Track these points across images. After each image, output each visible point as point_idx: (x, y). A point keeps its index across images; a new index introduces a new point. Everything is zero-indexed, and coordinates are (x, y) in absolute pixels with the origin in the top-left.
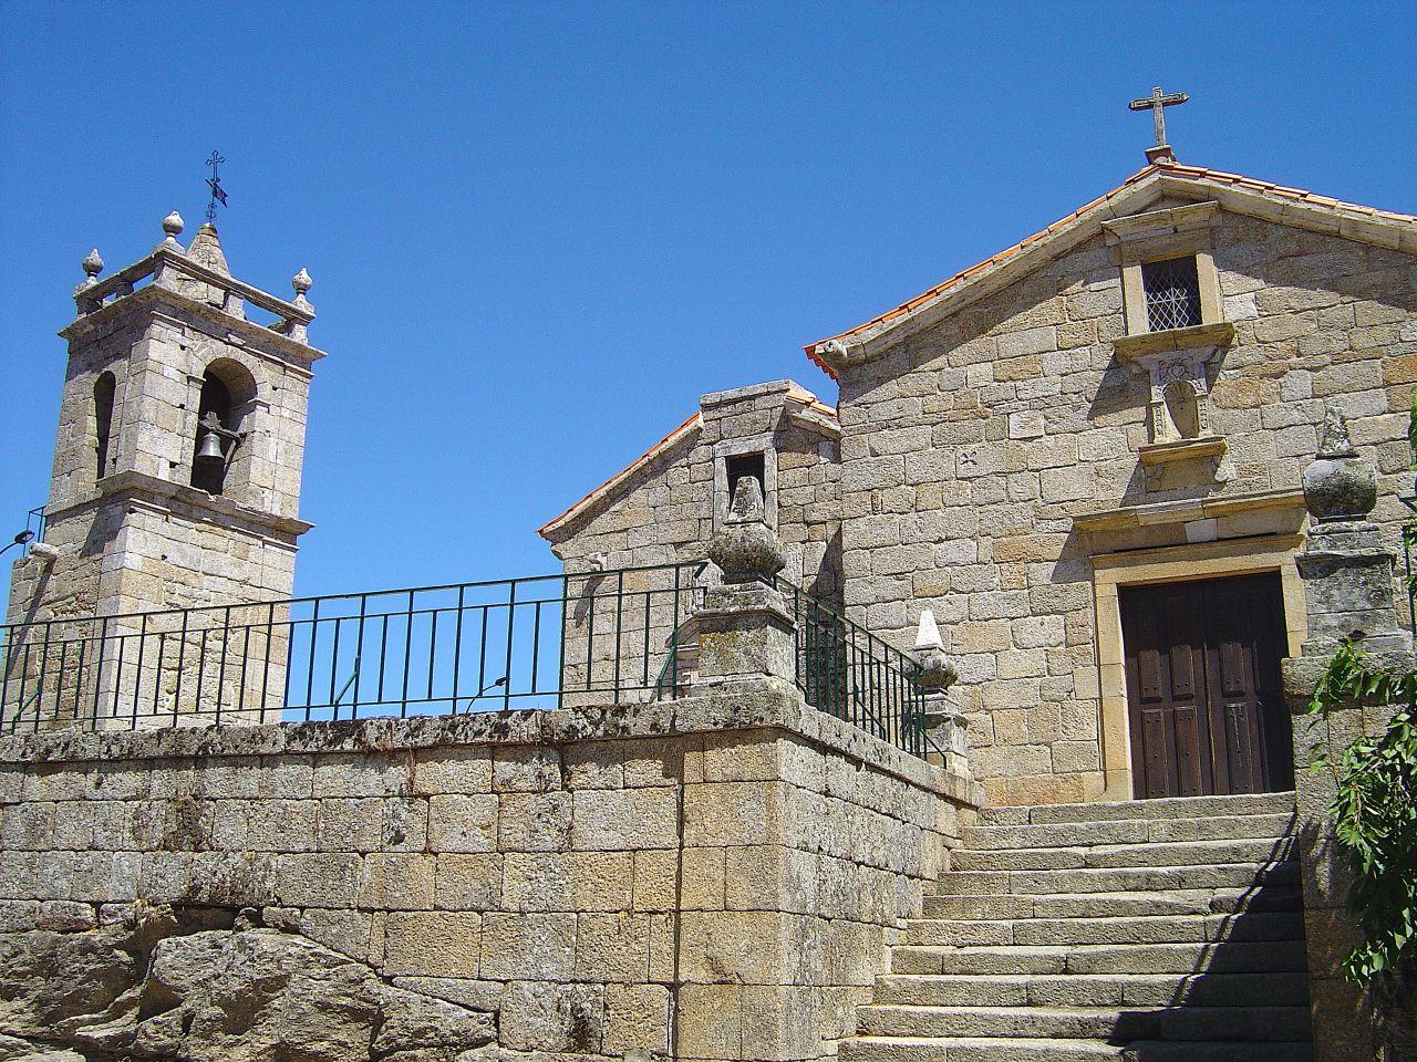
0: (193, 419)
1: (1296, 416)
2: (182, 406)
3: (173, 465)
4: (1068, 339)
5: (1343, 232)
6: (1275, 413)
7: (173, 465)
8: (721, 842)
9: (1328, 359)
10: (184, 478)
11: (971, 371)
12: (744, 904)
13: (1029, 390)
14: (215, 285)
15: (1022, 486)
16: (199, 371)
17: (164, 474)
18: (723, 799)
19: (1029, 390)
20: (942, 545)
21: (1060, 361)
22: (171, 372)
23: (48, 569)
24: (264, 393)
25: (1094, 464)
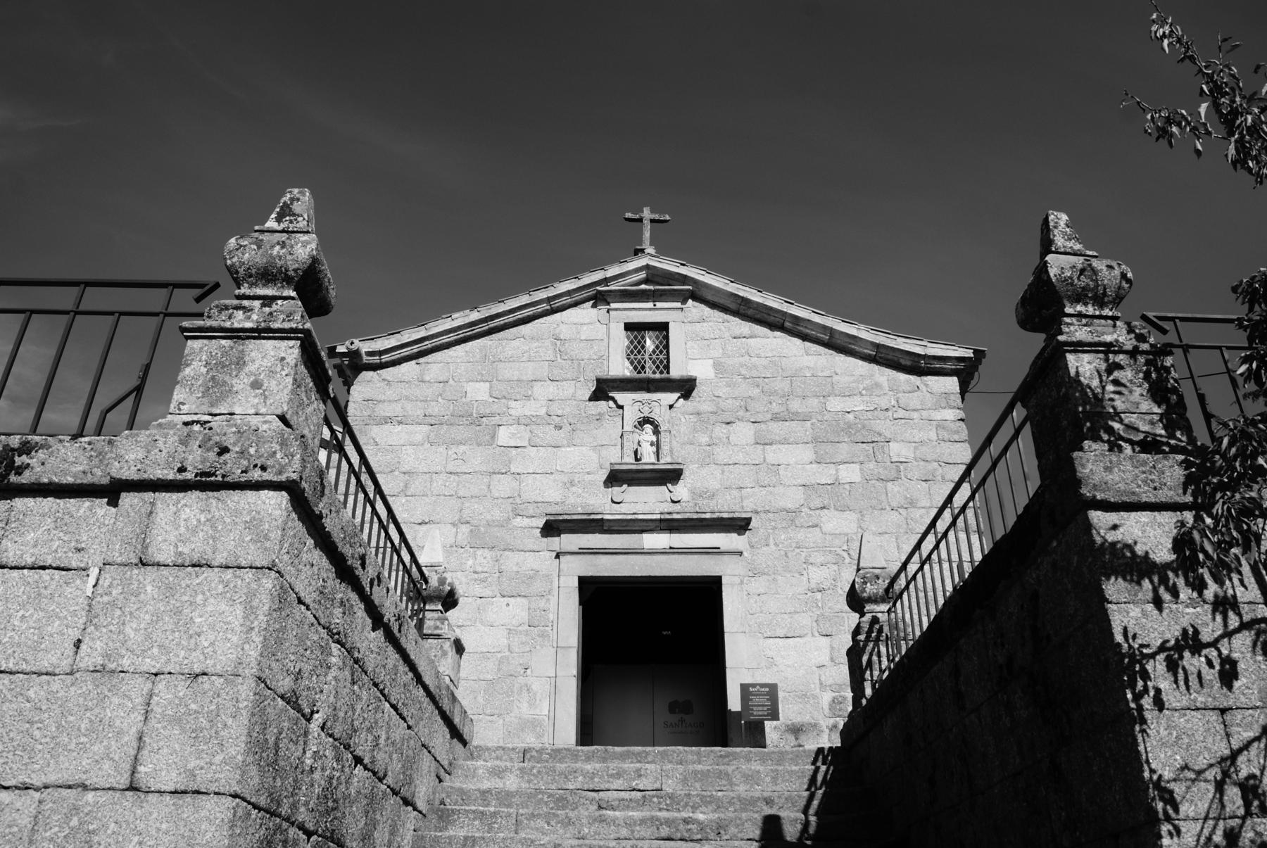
1: (740, 457)
4: (557, 373)
5: (787, 324)
6: (722, 454)
8: (149, 665)
9: (769, 416)
11: (470, 387)
12: (170, 780)
13: (517, 409)
15: (503, 486)
18: (170, 591)
19: (517, 409)
20: (424, 527)
21: (551, 389)
25: (572, 470)
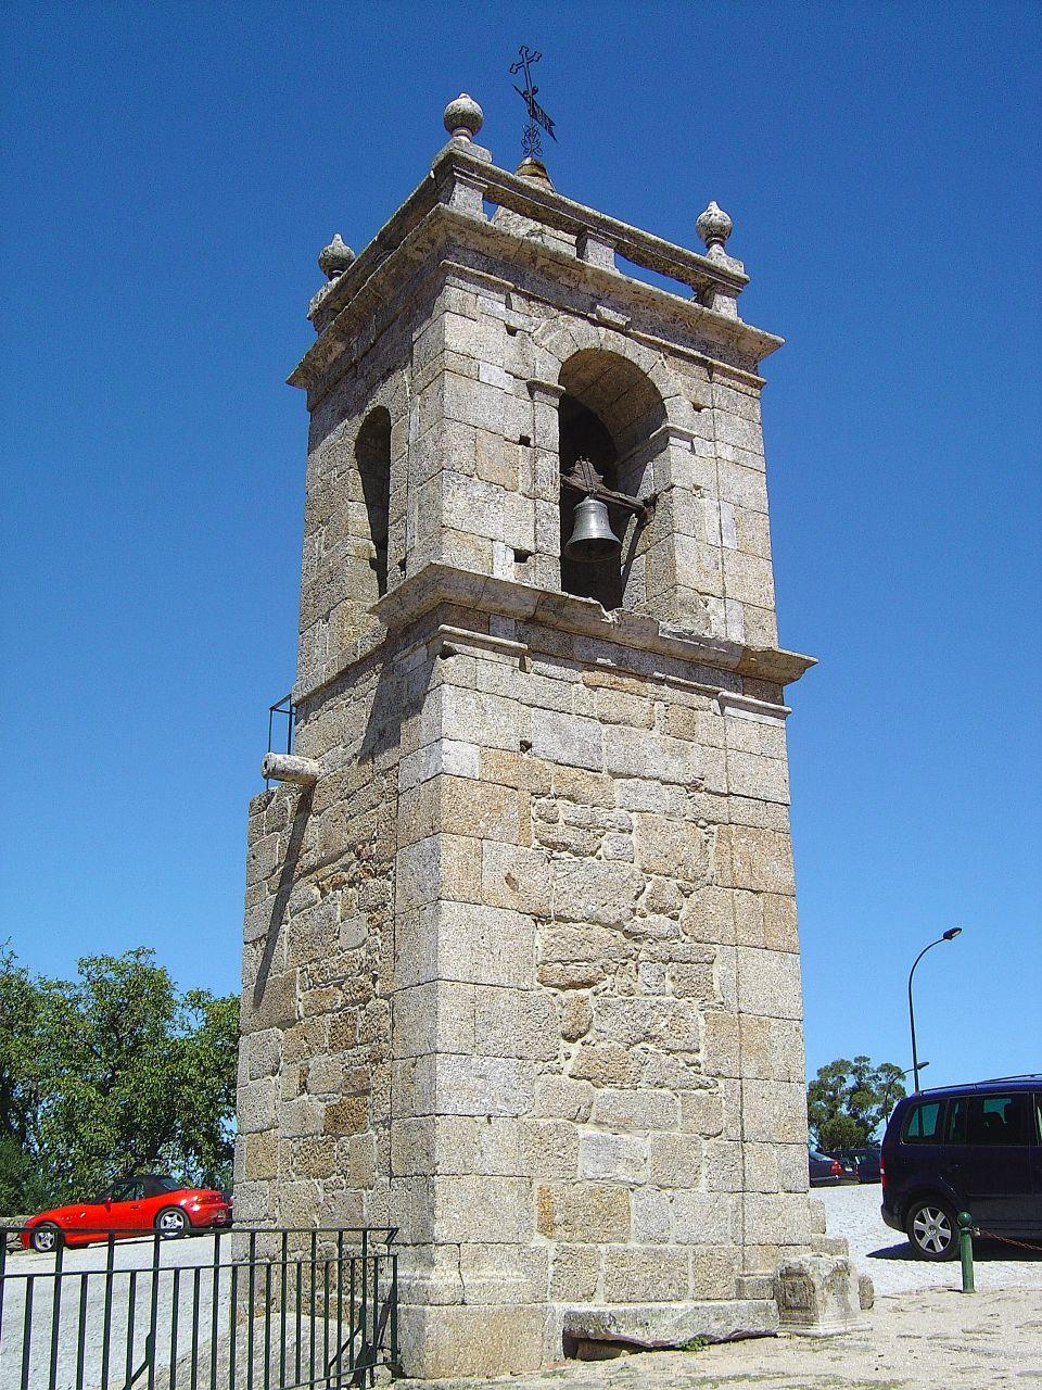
0: (550, 463)
2: (524, 441)
3: (521, 556)
7: (521, 556)
10: (547, 577)
14: (557, 224)
16: (548, 371)
17: (505, 570)
22: (492, 374)
23: (304, 807)
24: (679, 414)
